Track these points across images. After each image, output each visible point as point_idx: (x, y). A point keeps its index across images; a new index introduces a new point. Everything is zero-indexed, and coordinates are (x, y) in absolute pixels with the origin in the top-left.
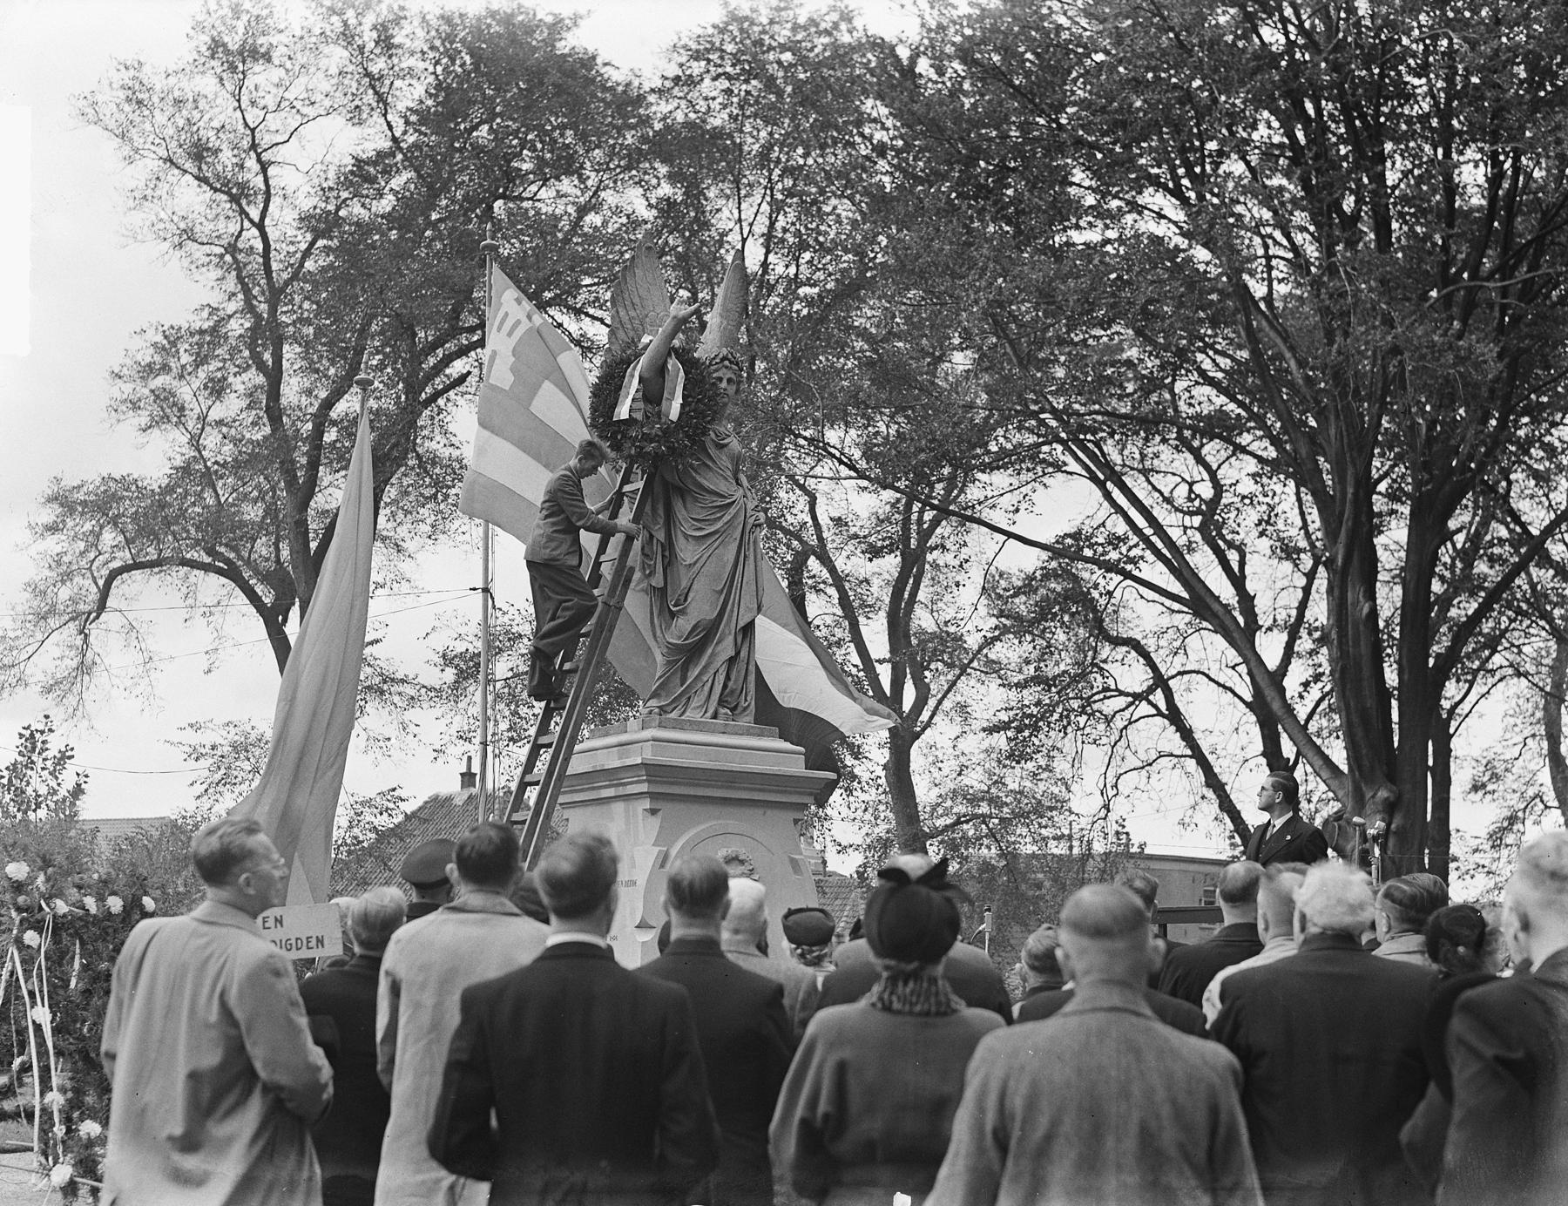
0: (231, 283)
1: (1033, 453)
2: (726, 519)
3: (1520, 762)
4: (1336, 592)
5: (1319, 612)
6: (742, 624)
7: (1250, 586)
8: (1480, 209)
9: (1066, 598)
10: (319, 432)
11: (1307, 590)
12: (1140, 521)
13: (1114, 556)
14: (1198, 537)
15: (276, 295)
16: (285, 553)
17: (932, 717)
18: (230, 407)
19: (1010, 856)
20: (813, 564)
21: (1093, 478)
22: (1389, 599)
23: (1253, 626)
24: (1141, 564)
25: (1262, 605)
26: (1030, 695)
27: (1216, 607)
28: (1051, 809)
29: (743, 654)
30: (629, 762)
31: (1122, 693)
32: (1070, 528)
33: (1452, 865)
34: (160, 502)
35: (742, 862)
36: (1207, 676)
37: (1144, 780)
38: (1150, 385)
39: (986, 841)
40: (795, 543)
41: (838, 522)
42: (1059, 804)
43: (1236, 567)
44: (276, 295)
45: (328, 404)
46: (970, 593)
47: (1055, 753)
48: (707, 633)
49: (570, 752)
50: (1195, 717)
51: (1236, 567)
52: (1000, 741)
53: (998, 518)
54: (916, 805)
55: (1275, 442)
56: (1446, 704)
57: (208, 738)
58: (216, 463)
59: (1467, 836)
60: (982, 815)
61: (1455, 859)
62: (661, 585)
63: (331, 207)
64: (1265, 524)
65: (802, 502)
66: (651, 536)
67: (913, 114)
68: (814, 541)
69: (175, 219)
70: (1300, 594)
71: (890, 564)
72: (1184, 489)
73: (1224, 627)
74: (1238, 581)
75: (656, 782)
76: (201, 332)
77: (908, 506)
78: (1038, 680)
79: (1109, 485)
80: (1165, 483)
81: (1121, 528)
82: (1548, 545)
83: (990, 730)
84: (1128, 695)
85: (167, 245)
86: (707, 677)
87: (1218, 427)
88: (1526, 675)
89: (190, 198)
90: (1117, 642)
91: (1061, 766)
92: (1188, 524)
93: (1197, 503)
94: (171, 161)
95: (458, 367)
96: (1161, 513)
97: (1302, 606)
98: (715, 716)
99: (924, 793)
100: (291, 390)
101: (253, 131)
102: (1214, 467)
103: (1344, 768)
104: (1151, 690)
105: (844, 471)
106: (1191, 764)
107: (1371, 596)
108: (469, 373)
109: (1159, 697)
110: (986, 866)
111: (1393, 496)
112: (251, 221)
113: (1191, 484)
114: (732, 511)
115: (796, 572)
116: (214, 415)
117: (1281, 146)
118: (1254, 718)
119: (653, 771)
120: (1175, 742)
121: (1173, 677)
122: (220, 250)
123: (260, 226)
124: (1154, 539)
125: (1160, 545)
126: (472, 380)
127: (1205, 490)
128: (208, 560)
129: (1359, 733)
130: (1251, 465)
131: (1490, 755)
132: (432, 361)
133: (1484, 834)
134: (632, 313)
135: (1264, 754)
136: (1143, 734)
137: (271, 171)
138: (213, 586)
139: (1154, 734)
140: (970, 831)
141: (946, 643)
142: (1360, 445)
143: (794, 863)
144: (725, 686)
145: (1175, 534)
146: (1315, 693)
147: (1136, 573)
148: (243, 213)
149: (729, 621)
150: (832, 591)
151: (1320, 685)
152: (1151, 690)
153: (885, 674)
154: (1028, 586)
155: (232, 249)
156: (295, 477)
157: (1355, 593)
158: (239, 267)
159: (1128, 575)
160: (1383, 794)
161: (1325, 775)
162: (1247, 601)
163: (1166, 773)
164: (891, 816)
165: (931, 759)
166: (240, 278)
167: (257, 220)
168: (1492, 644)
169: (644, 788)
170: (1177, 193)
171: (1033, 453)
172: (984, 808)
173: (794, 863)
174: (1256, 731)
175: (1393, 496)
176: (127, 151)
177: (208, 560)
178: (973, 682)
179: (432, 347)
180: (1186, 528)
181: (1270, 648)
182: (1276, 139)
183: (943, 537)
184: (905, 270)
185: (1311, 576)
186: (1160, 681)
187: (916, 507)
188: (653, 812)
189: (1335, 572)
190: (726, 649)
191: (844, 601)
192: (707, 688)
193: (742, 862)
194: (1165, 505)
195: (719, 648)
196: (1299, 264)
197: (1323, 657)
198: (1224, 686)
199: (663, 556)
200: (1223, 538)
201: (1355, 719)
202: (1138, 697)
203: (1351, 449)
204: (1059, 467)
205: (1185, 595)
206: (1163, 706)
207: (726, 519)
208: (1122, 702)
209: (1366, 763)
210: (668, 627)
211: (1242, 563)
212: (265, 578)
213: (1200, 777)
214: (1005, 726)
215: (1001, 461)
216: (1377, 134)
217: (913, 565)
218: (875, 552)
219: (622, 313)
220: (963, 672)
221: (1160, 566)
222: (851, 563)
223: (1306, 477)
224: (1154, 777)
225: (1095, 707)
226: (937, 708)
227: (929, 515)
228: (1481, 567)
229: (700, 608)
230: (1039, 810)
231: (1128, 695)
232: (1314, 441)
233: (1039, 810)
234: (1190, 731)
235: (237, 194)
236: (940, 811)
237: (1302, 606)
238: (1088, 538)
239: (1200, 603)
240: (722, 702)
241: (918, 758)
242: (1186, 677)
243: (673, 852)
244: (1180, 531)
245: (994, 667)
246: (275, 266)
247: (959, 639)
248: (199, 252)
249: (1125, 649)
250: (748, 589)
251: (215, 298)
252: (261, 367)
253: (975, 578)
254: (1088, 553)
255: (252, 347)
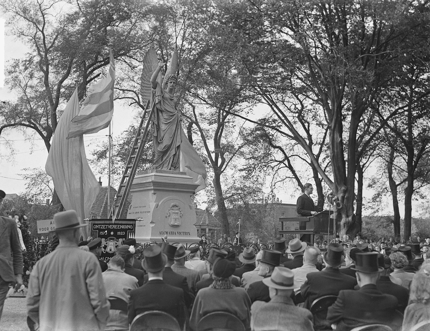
0: (34, 48)
1: (253, 97)
2: (173, 119)
3: (381, 179)
4: (332, 135)
5: (328, 140)
6: (177, 146)
7: (311, 133)
8: (370, 34)
9: (261, 136)
10: (59, 89)
11: (326, 134)
12: (281, 115)
13: (274, 125)
14: (297, 120)
15: (47, 51)
16: (50, 123)
17: (226, 167)
18: (35, 82)
19: (246, 204)
20: (194, 126)
21: (269, 104)
22: (346, 135)
23: (311, 143)
24: (281, 127)
25: (313, 138)
26: (251, 162)
27: (301, 139)
28: (257, 192)
29: (177, 153)
30: (148, 181)
31: (277, 161)
32: (263, 117)
33: (363, 207)
34: (15, 108)
35: (177, 206)
36: (299, 156)
37: (282, 184)
38: (284, 79)
39: (240, 200)
40: (189, 120)
41: (201, 114)
42: (260, 190)
43: (307, 127)
44: (47, 51)
45: (62, 82)
46: (236, 134)
47: (258, 177)
48: (168, 148)
49: (133, 178)
50: (295, 168)
51: (307, 127)
52: (244, 173)
53: (243, 114)
54: (221, 190)
55: (317, 95)
56: (361, 164)
57: (29, 173)
58: (30, 97)
59: (367, 199)
60: (239, 193)
61: (364, 205)
62: (156, 135)
63: (62, 26)
64: (314, 117)
65: (191, 109)
66: (154, 123)
67: (222, 6)
68: (194, 119)
69: (18, 29)
70: (324, 134)
71: (215, 126)
72: (293, 106)
73: (304, 145)
74: (307, 131)
75: (156, 186)
76: (26, 61)
77: (220, 112)
78: (253, 158)
79: (273, 106)
80: (289, 105)
81: (276, 117)
82: (388, 122)
83: (241, 170)
84: (278, 161)
85: (15, 36)
86: (168, 159)
87: (302, 90)
88: (381, 156)
89: (23, 24)
90: (275, 147)
91: (260, 180)
92: (294, 116)
93: (297, 110)
94: (17, 13)
95: (96, 72)
96: (287, 113)
97: (325, 138)
98: (170, 169)
99: (224, 188)
100: (52, 77)
101: (40, 5)
102: (302, 100)
103: (333, 181)
104: (284, 160)
105: (202, 102)
106: (294, 180)
107: (341, 136)
108: (100, 73)
109: (286, 162)
110: (240, 207)
111: (348, 110)
112: (40, 30)
113: (295, 105)
114: (175, 117)
115: (189, 128)
116: (29, 84)
117: (319, 15)
118: (311, 167)
119: (155, 183)
120: (290, 174)
121: (290, 157)
122: (31, 38)
123: (42, 32)
124: (285, 121)
125: (286, 122)
126: (101, 75)
127: (299, 107)
128: (28, 123)
129: (337, 172)
130: (311, 101)
131: (373, 177)
132: (90, 70)
133: (371, 198)
134: (148, 65)
135: (314, 177)
136: (282, 172)
137: (45, 16)
138: (30, 131)
139: (285, 172)
140: (235, 197)
141: (229, 148)
142: (339, 97)
143: (190, 206)
144: (173, 162)
145: (290, 119)
146: (327, 161)
147: (280, 130)
148: (37, 27)
149: (174, 145)
150: (199, 133)
151: (328, 159)
152: (284, 160)
153: (213, 156)
154: (252, 132)
155: (34, 37)
156: (52, 101)
157: (337, 135)
158: (36, 42)
159: (278, 130)
160: (343, 188)
161: (328, 183)
162: (310, 136)
163: (288, 182)
164: (215, 194)
165: (225, 178)
166: (37, 46)
167: (41, 30)
168: (374, 148)
169: (152, 188)
170: (292, 29)
171: (253, 97)
172: (240, 192)
173: (190, 206)
174: (312, 170)
175: (348, 110)
176: (4, 9)
177: (28, 123)
178: (236, 158)
179: (90, 66)
180: (294, 117)
181: (316, 150)
182: (318, 13)
183: (229, 119)
184: (219, 48)
185: (327, 130)
186: (287, 158)
187: (221, 111)
188: (154, 194)
189: (331, 130)
190: (173, 152)
191: (202, 136)
192: (168, 162)
193: (177, 206)
194: (289, 111)
195: (171, 152)
196: (324, 48)
197: (328, 152)
198: (303, 159)
199: (157, 128)
200: (304, 119)
201: (336, 169)
202: (281, 162)
203: (336, 98)
204: (260, 101)
205: (292, 135)
206: (287, 165)
207: (173, 119)
208: (276, 163)
209: (339, 180)
210: (158, 146)
211: (309, 126)
212: (44, 129)
213: (297, 183)
214: (244, 169)
215: (246, 98)
216: (345, 13)
217: (221, 125)
218: (210, 123)
219: (146, 64)
220: (234, 155)
221: (287, 128)
222: (204, 125)
223: (325, 106)
224: (285, 183)
225: (269, 164)
226: (227, 165)
227: (224, 114)
228: (371, 128)
229: (166, 142)
230: (254, 192)
231: (278, 161)
232: (326, 94)
233: (254, 192)
234: (294, 171)
235: (36, 23)
236: (228, 192)
237: (325, 138)
238: (267, 120)
239: (297, 137)
240: (172, 166)
241: (222, 178)
242: (294, 157)
243: (160, 204)
244: (292, 118)
245: (242, 154)
246: (46, 42)
247: (233, 147)
248: (26, 39)
249: (277, 149)
250: (179, 137)
251: (30, 51)
252: (43, 71)
253: (237, 129)
254: (267, 124)
255: (40, 65)
